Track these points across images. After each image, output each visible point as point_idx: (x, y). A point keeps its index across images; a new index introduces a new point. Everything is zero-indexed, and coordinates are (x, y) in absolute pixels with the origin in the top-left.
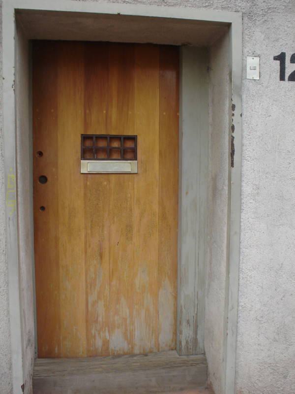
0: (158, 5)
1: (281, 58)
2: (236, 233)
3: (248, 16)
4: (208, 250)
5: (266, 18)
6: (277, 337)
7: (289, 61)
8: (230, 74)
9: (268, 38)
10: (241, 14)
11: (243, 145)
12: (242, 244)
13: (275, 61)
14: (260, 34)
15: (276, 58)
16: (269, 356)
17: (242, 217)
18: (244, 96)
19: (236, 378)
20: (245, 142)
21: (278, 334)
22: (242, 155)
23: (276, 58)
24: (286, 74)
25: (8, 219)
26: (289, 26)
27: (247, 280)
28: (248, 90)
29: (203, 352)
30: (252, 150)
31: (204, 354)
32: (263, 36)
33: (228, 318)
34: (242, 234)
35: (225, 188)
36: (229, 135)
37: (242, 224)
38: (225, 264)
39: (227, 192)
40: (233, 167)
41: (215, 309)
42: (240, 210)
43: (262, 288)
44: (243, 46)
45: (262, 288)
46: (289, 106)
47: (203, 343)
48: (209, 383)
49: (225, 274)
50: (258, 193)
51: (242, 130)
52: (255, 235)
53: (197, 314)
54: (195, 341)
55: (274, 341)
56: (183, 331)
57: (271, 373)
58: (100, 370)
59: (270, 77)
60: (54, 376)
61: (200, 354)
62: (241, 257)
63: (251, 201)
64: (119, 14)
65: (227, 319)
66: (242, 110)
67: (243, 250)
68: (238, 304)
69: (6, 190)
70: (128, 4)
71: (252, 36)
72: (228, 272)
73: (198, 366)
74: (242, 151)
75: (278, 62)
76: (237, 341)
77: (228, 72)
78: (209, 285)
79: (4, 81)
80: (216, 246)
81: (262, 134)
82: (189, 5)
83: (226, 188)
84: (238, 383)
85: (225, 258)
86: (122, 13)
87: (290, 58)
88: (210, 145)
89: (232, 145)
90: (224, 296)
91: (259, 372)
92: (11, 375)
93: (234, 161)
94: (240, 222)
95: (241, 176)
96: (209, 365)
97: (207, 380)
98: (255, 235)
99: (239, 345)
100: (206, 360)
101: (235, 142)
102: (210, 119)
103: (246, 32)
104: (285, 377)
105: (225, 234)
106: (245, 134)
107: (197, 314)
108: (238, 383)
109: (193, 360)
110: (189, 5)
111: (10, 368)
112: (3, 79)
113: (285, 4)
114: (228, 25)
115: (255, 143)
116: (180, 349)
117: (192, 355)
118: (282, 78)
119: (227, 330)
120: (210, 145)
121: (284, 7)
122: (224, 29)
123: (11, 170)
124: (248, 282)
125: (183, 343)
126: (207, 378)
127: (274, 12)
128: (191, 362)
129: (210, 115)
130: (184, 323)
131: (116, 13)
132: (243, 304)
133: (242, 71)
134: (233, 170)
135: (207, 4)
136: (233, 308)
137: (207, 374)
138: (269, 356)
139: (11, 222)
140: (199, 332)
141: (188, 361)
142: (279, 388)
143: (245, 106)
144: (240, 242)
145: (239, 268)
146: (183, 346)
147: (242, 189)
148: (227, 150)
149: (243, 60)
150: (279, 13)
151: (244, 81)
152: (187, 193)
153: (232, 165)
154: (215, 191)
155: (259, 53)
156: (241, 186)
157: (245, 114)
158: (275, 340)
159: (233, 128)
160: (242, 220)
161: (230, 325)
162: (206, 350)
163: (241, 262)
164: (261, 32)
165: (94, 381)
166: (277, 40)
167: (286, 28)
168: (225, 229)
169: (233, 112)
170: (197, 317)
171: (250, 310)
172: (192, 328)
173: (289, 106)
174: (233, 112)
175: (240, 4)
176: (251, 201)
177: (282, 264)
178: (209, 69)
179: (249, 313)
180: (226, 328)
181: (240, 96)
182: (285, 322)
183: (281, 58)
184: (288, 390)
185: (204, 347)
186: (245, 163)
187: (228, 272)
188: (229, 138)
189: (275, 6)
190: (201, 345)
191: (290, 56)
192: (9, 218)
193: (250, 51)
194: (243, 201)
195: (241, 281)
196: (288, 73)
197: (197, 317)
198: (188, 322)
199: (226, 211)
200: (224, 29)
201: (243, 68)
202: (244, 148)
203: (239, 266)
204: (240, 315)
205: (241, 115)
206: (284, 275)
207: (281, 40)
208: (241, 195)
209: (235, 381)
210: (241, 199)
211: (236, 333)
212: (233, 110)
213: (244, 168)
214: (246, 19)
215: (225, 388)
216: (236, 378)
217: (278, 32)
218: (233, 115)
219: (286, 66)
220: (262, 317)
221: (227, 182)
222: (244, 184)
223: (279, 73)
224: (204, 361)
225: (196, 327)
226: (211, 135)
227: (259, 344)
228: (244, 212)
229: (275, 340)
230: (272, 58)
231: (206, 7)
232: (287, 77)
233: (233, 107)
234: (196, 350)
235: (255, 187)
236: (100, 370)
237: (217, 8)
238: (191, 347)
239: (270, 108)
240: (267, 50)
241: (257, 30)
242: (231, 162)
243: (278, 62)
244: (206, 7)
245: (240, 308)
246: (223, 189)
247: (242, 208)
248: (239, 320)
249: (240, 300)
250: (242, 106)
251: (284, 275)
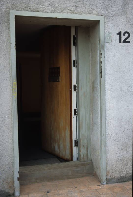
0: (71, 14)
1: (120, 34)
2: (104, 104)
3: (107, 17)
4: (91, 114)
5: (113, 18)
6: (122, 148)
7: (123, 35)
8: (100, 40)
9: (114, 26)
10: (103, 17)
11: (105, 69)
12: (106, 109)
13: (117, 35)
14: (111, 24)
15: (117, 34)
16: (119, 156)
17: (106, 98)
18: (105, 50)
19: (106, 166)
20: (106, 68)
21: (123, 146)
22: (105, 73)
23: (117, 34)
24: (122, 40)
25: (13, 100)
26: (123, 21)
27: (109, 124)
28: (107, 47)
29: (90, 160)
30: (109, 71)
31: (91, 160)
32: (112, 25)
33: (102, 139)
34: (106, 105)
35: (98, 86)
36: (100, 65)
37: (106, 101)
38: (100, 118)
39: (99, 88)
40: (102, 78)
41: (96, 138)
42: (105, 95)
43: (115, 127)
44: (105, 29)
45: (115, 127)
46: (123, 53)
47: (91, 156)
48: (94, 172)
49: (100, 122)
50: (112, 88)
51: (105, 63)
52: (111, 105)
53: (87, 142)
54: (87, 154)
55: (121, 150)
56: (82, 150)
57: (121, 164)
58: (47, 169)
59: (115, 41)
60: (27, 172)
61: (89, 161)
62: (106, 114)
63: (109, 91)
64: (56, 18)
65: (101, 140)
66: (105, 55)
67: (107, 111)
68: (106, 134)
69: (13, 88)
70: (59, 13)
71: (108, 25)
72: (101, 120)
73: (89, 165)
74: (105, 71)
75: (118, 35)
76: (106, 149)
77: (98, 40)
78: (92, 129)
79: (11, 44)
80: (95, 111)
81: (113, 64)
82: (83, 13)
83: (99, 86)
84: (107, 168)
85: (99, 115)
86: (57, 17)
87: (123, 34)
88: (90, 69)
89: (101, 69)
90: (100, 131)
91: (116, 163)
92: (13, 168)
93: (102, 76)
94: (105, 100)
95: (105, 81)
96: (94, 165)
97: (93, 172)
98: (111, 105)
99: (107, 151)
100: (92, 163)
101: (102, 68)
102: (90, 58)
103: (106, 24)
104: (127, 165)
105: (99, 105)
106: (106, 64)
107: (87, 142)
108: (107, 168)
109: (86, 163)
110: (83, 13)
111: (13, 165)
112: (11, 44)
113: (121, 12)
114: (99, 21)
115: (110, 68)
116: (81, 159)
117: (86, 161)
118: (120, 42)
119: (102, 144)
120: (90, 69)
121: (120, 13)
122: (97, 23)
123: (15, 80)
124: (109, 124)
125: (82, 156)
126: (93, 170)
127: (116, 15)
128: (86, 164)
129: (90, 54)
130: (82, 147)
131: (55, 17)
132: (108, 134)
133: (104, 39)
134: (102, 79)
135: (90, 13)
136: (104, 135)
137: (93, 169)
138: (119, 156)
139: (15, 102)
140: (88, 151)
141: (85, 164)
142: (125, 170)
143: (105, 53)
144: (105, 108)
145: (106, 119)
146: (82, 158)
147: (105, 86)
148: (99, 71)
149: (105, 35)
150: (118, 15)
151: (105, 43)
152: (81, 89)
153: (101, 77)
154: (93, 88)
155: (111, 32)
156: (105, 85)
157: (106, 57)
158: (122, 149)
159: (101, 62)
160: (106, 99)
161: (103, 143)
162: (92, 158)
163: (106, 116)
164: (111, 23)
165: (44, 174)
166: (118, 27)
167: (121, 22)
168: (99, 103)
169: (101, 56)
170: (87, 144)
171: (111, 136)
172: (85, 149)
173: (123, 53)
174: (101, 56)
175: (103, 13)
176: (109, 91)
177: (123, 117)
178: (89, 36)
179: (111, 138)
180: (101, 144)
181: (104, 50)
182: (125, 141)
183: (120, 34)
184: (129, 171)
185: (91, 157)
186: (106, 76)
187: (101, 120)
188: (100, 66)
189: (117, 13)
190: (89, 157)
191: (123, 33)
192: (14, 100)
193: (107, 31)
194: (106, 91)
195: (107, 124)
196: (122, 40)
197: (87, 144)
198: (84, 146)
199: (99, 96)
200: (97, 23)
201: (104, 38)
202: (106, 70)
203: (106, 118)
204: (107, 138)
205: (104, 57)
206: (124, 122)
207: (119, 27)
208: (105, 89)
209: (106, 167)
210: (105, 91)
211: (106, 146)
212: (101, 55)
213: (106, 78)
214: (105, 18)
215: (102, 170)
216: (106, 166)
217: (118, 23)
218: (101, 57)
219: (122, 37)
220: (116, 139)
221: (99, 84)
222: (106, 85)
223: (119, 40)
224: (92, 163)
225: (87, 148)
226: (91, 64)
227: (115, 151)
228: (106, 96)
229: (122, 149)
230: (116, 34)
231: (89, 14)
232: (122, 42)
233: (101, 54)
234: (87, 159)
235: (110, 86)
236: (47, 169)
237: (94, 14)
238: (85, 158)
239: (116, 54)
240: (114, 30)
241: (110, 23)
242: (101, 76)
243: (118, 35)
244: (89, 14)
245: (107, 135)
246: (97, 87)
247: (106, 94)
248: (106, 140)
249: (106, 132)
250: (105, 53)
251: (124, 122)
